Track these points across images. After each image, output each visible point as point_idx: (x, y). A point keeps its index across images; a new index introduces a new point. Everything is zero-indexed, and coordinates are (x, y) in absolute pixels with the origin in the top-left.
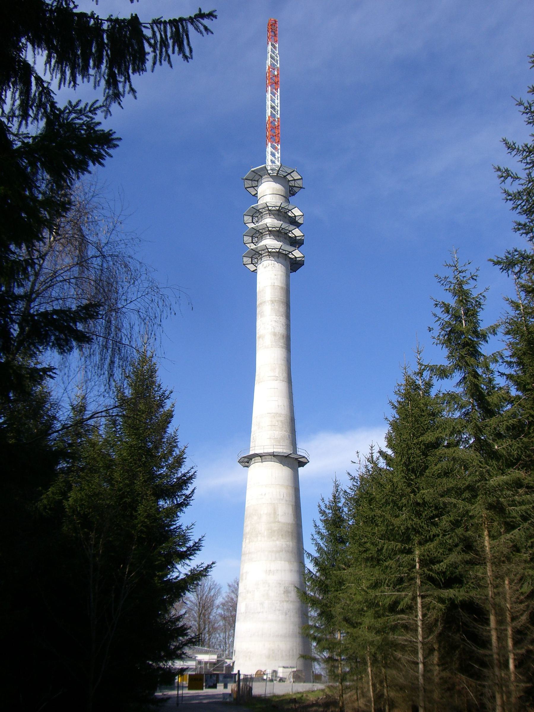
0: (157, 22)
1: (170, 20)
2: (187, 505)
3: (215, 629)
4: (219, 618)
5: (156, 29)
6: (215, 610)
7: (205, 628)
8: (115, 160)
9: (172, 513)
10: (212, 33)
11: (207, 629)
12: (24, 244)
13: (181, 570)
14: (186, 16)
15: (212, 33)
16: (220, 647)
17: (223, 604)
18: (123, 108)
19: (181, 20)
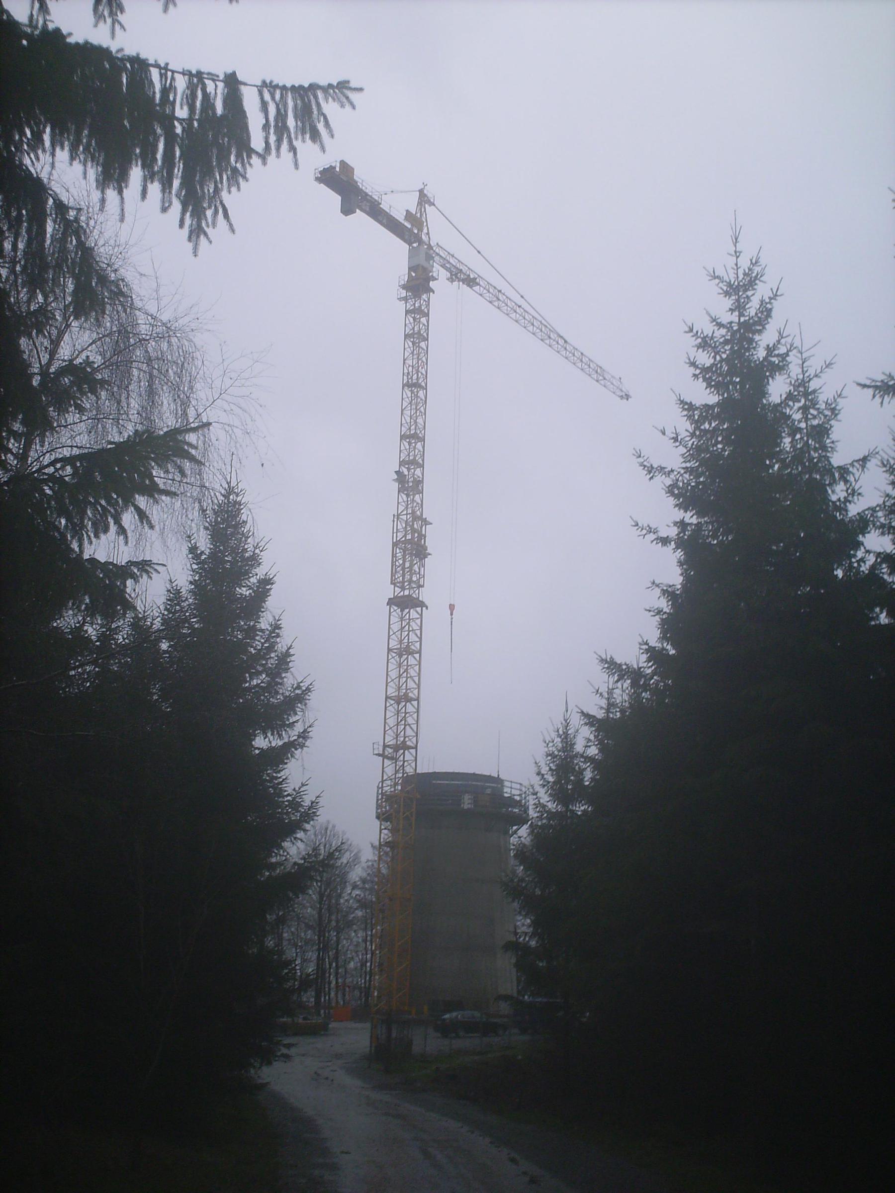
0: (267, 86)
1: (293, 86)
2: (302, 746)
3: (350, 924)
4: (355, 906)
5: (267, 97)
6: (349, 890)
7: (330, 921)
8: (313, 699)
9: (278, 757)
10: (354, 107)
11: (333, 923)
12: (155, 123)
13: (294, 850)
14: (323, 83)
15: (354, 107)
16: (358, 956)
17: (364, 881)
18: (233, 231)
19: (313, 87)
